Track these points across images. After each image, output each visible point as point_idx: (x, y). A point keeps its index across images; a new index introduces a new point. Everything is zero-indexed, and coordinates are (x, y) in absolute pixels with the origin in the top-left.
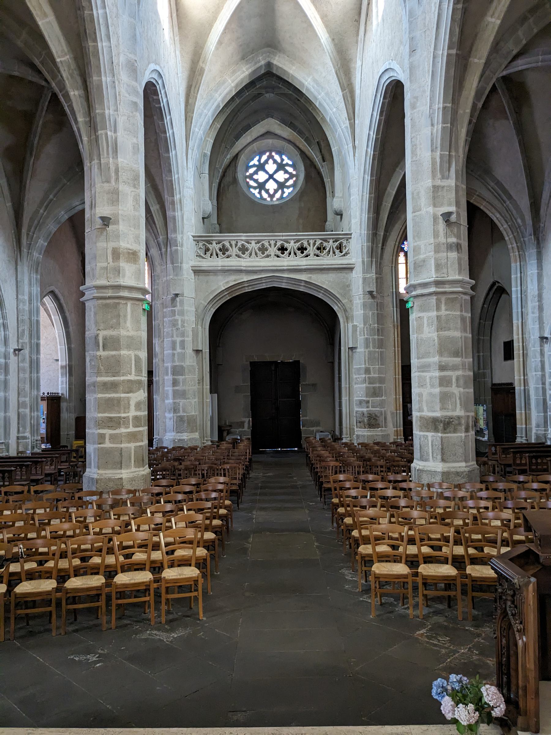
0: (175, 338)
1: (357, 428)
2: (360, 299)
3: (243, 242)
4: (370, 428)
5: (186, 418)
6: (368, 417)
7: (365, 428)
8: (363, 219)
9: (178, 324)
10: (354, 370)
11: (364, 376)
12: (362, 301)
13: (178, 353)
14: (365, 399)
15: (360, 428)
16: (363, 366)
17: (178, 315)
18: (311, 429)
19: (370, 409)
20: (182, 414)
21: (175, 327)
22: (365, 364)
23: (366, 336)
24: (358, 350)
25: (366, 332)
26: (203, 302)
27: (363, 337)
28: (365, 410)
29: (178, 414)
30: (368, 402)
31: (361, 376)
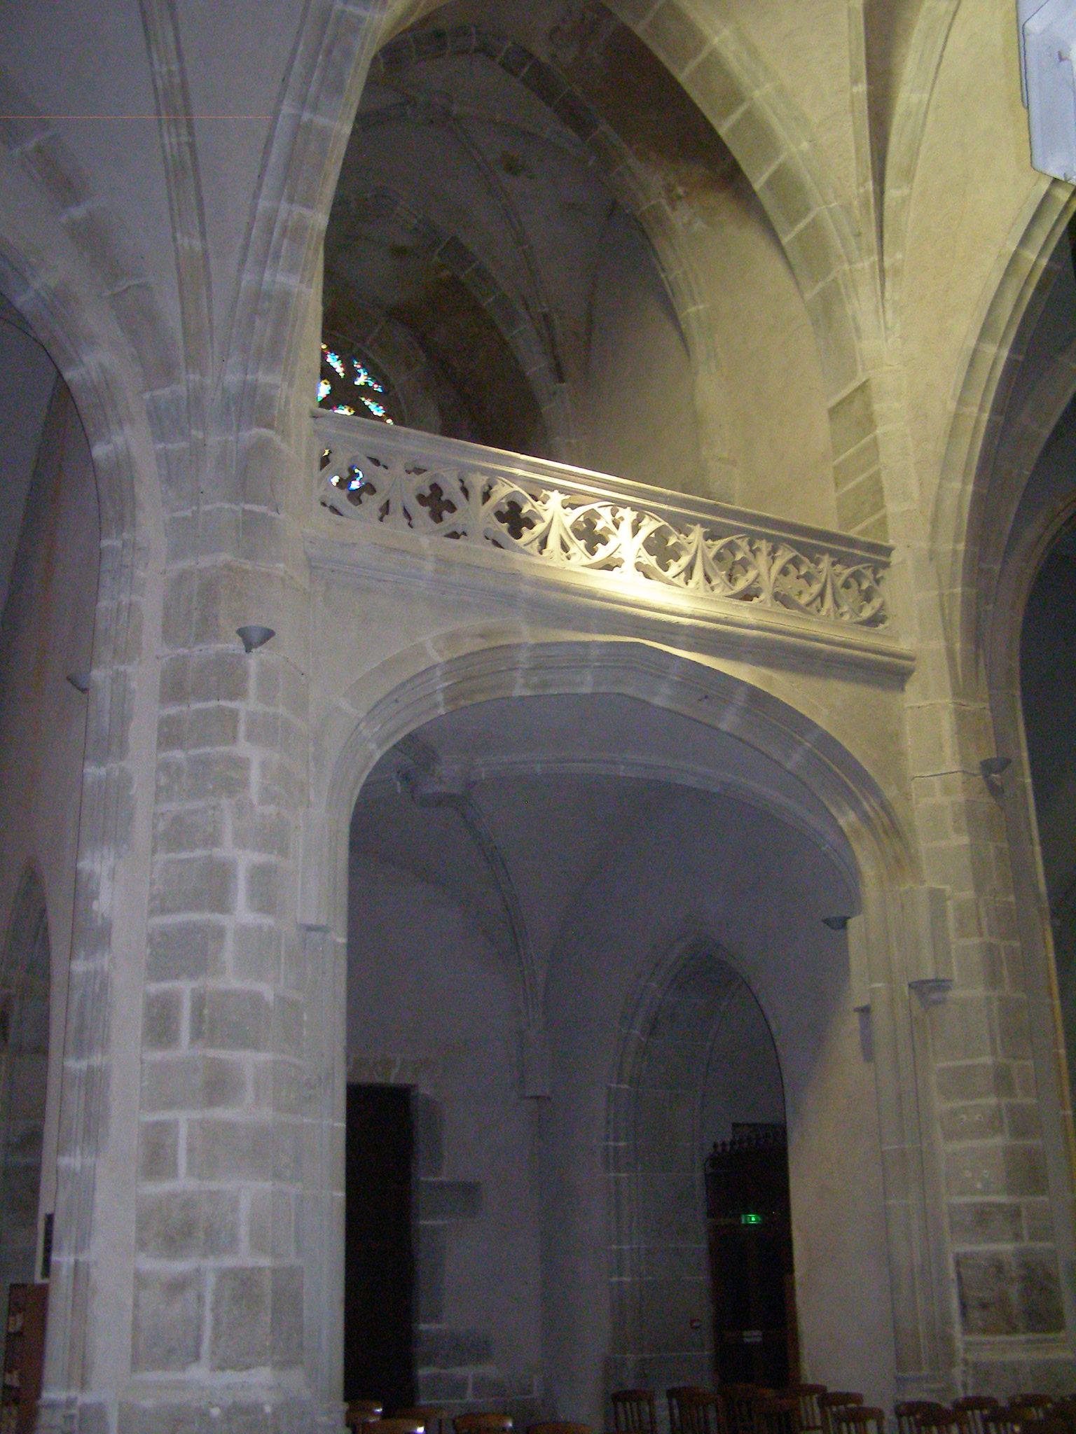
0: (226, 852)
1: (967, 1329)
2: (947, 790)
3: (516, 488)
4: (1034, 1330)
5: (268, 1285)
6: (1023, 1278)
7: (1013, 1329)
8: (581, 599)
9: (245, 783)
10: (933, 1079)
11: (992, 1100)
12: (960, 797)
13: (244, 932)
14: (1002, 1199)
15: (985, 1331)
16: (987, 1060)
17: (249, 737)
18: (459, 1372)
19: (1027, 1243)
20: (250, 1262)
21: (231, 794)
22: (994, 1053)
23: (987, 938)
24: (956, 993)
25: (984, 923)
26: (345, 705)
27: (976, 940)
28: (1006, 1247)
29: (229, 1262)
30: (1014, 1214)
31: (982, 1101)
